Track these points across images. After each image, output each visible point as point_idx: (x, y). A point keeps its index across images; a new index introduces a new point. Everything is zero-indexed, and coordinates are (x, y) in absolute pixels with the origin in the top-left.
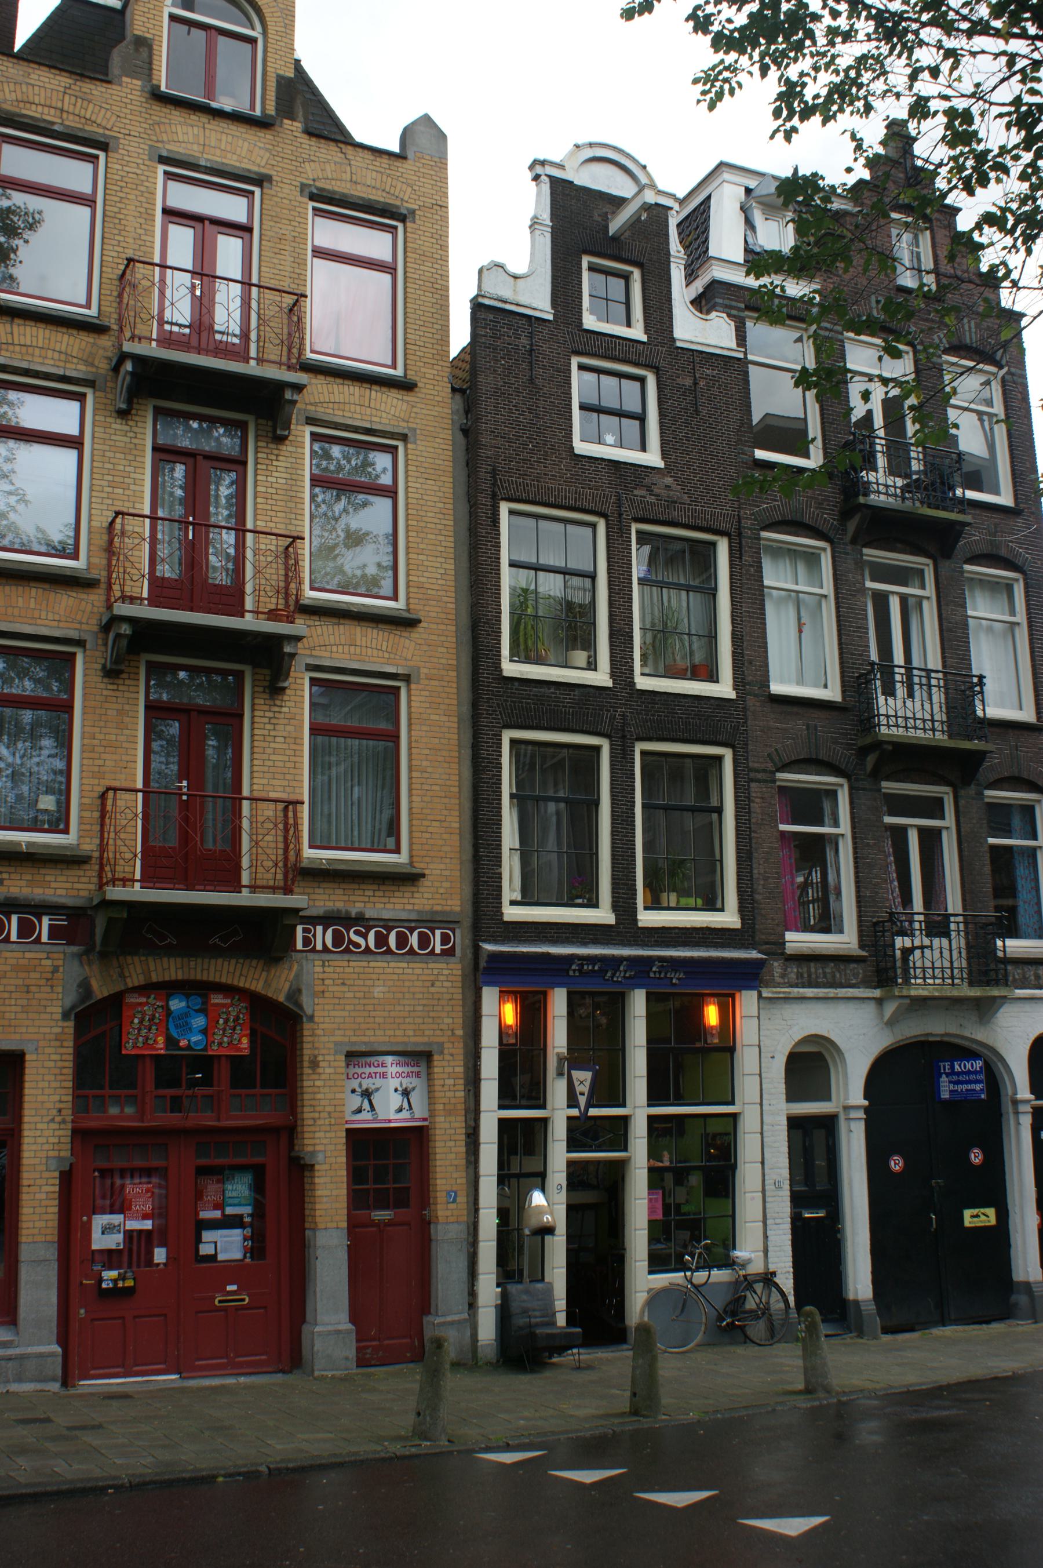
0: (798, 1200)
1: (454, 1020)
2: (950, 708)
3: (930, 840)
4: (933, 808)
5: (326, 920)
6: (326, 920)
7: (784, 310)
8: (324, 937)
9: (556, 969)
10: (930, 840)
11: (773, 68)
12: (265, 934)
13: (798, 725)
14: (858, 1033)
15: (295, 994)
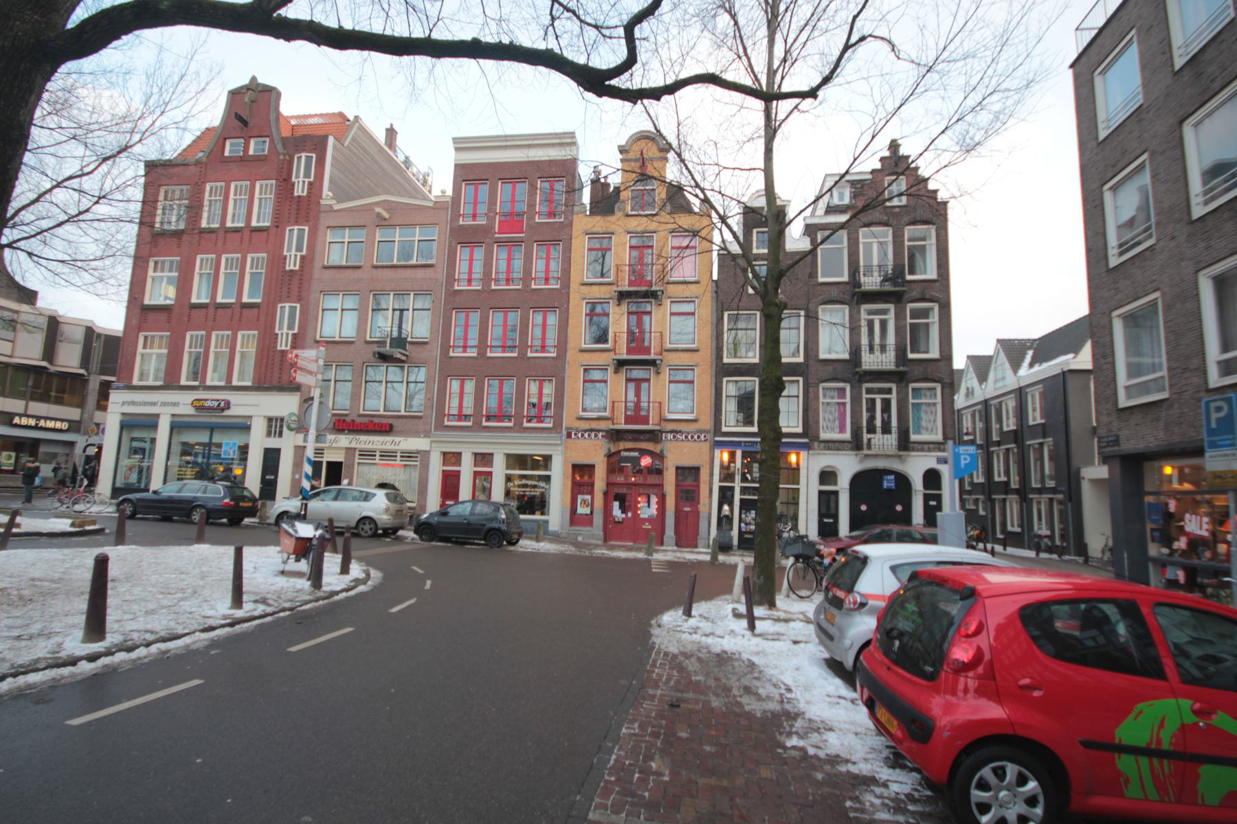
0: (821, 516)
1: (707, 458)
2: (897, 357)
3: (883, 324)
4: (885, 312)
5: (671, 432)
6: (671, 432)
7: (816, 558)
8: (670, 436)
9: (738, 444)
10: (883, 324)
11: (813, 535)
12: (654, 436)
13: (830, 368)
14: (847, 466)
15: (662, 451)
